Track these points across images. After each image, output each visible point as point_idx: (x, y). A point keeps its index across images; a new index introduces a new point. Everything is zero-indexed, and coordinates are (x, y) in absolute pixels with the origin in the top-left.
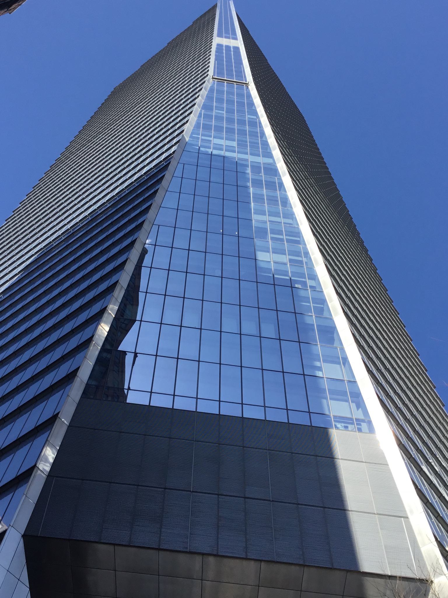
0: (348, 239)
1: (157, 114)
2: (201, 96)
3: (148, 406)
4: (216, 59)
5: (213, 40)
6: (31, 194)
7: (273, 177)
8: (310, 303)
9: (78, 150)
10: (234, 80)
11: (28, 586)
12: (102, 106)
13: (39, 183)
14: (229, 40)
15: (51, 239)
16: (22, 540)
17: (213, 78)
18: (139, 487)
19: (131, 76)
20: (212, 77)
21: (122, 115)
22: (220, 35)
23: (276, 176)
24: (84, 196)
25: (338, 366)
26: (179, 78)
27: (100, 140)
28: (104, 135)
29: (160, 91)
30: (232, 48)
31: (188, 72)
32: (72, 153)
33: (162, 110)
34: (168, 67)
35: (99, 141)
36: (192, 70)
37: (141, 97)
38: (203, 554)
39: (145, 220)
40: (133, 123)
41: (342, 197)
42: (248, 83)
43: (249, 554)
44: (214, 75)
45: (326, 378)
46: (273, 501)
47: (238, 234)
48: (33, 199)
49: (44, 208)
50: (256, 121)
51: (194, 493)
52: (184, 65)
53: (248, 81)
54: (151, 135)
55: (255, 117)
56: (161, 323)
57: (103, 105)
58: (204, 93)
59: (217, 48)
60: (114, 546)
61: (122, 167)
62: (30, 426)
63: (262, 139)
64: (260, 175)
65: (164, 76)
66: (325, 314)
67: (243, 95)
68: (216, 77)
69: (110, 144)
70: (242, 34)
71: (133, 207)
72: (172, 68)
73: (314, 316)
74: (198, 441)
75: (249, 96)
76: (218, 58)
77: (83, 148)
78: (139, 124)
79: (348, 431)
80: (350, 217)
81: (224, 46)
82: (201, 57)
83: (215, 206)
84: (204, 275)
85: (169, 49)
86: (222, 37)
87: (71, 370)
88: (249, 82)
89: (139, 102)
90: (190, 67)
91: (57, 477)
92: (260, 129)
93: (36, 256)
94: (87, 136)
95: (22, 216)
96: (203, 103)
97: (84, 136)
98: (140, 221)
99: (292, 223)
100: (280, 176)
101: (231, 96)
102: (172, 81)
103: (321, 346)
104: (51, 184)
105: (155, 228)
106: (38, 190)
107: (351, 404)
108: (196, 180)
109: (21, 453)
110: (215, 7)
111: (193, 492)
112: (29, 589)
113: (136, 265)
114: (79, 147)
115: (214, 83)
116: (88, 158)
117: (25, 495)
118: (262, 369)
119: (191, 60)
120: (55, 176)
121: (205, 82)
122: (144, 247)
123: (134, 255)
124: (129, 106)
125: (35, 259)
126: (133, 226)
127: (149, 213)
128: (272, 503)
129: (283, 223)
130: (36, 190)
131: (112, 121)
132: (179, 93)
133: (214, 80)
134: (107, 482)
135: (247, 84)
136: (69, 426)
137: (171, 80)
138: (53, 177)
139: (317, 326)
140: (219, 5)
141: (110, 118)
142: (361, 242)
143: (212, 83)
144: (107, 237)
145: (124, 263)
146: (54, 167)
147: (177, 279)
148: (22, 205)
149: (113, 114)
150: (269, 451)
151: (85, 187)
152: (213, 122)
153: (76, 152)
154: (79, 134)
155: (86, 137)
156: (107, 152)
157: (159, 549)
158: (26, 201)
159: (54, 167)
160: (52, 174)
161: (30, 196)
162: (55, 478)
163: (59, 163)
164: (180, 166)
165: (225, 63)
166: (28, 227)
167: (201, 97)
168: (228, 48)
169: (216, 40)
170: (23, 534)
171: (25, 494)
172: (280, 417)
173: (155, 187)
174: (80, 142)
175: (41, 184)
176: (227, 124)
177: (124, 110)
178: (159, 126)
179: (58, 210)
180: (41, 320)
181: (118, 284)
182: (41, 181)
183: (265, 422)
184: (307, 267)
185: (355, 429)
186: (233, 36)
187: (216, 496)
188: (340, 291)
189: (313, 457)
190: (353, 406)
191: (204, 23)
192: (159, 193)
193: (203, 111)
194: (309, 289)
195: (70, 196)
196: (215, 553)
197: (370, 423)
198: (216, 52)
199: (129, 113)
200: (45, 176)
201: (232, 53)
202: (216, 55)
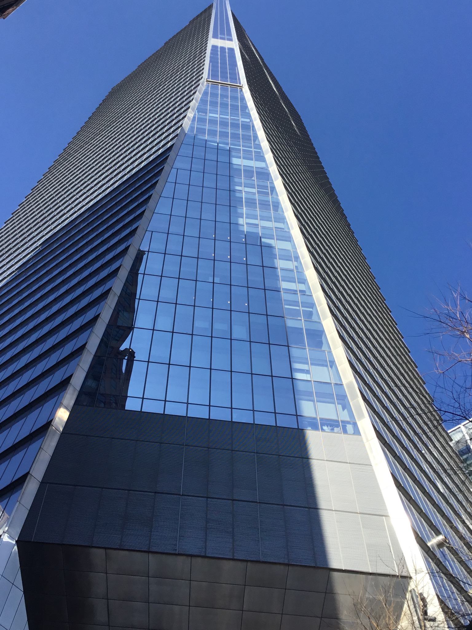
0: (342, 236)
3: (185, 416)
4: (210, 61)
5: (208, 42)
6: (29, 196)
7: (266, 181)
8: (299, 306)
10: (228, 82)
12: (99, 107)
13: (38, 185)
14: (225, 41)
17: (207, 81)
18: (130, 492)
19: (132, 73)
20: (206, 80)
21: (124, 112)
22: (215, 36)
23: (269, 181)
25: (325, 368)
26: (199, 60)
28: (81, 156)
29: (150, 97)
30: (227, 49)
32: (70, 155)
33: (164, 107)
34: (165, 67)
35: (108, 134)
36: (194, 67)
37: (137, 98)
39: (138, 227)
41: (337, 196)
42: (241, 85)
43: (235, 554)
44: (208, 78)
45: (313, 381)
46: (259, 503)
47: (230, 240)
48: (31, 201)
50: (248, 124)
51: (183, 497)
52: (174, 71)
54: (139, 144)
55: (248, 120)
56: (153, 330)
57: (100, 106)
58: (198, 96)
59: (212, 50)
60: (106, 551)
61: (126, 165)
63: (255, 142)
64: (252, 179)
65: (153, 85)
66: (314, 318)
67: (237, 98)
68: (210, 80)
69: (107, 146)
70: (237, 34)
71: (117, 220)
72: (167, 73)
73: (303, 320)
75: (243, 99)
76: (213, 60)
77: (80, 149)
79: (334, 433)
80: (344, 217)
81: (219, 48)
84: (196, 281)
85: (166, 50)
88: (243, 85)
89: (135, 103)
91: (50, 483)
92: (253, 132)
93: (8, 278)
94: (85, 138)
95: (21, 218)
96: (197, 107)
97: (85, 133)
98: (134, 227)
99: (283, 227)
100: (272, 180)
101: (225, 99)
103: (309, 350)
105: (148, 234)
106: (48, 184)
107: (337, 405)
108: (189, 185)
109: (17, 458)
110: (211, 7)
111: (182, 495)
112: (23, 593)
113: (129, 272)
114: (77, 148)
115: (208, 86)
117: (18, 502)
119: (198, 53)
120: (70, 165)
121: (199, 85)
122: (139, 248)
123: (127, 262)
124: (132, 103)
125: (6, 283)
126: (131, 217)
128: (258, 504)
130: (35, 192)
131: (131, 105)
133: (208, 83)
134: (99, 487)
137: (162, 87)
138: (52, 179)
139: (306, 330)
140: (214, 5)
141: (113, 116)
142: (354, 241)
143: (206, 86)
145: (118, 269)
146: (52, 168)
147: (169, 286)
148: (20, 208)
149: (110, 116)
150: (257, 454)
153: (74, 154)
154: (77, 135)
155: (84, 139)
156: (104, 155)
157: (149, 552)
158: (24, 203)
159: (52, 168)
160: (50, 176)
161: (29, 198)
162: (48, 484)
163: (57, 165)
165: (219, 65)
166: (26, 230)
167: (195, 101)
168: (223, 49)
169: (212, 42)
171: (19, 501)
172: (268, 420)
173: (149, 192)
174: (78, 144)
175: (39, 186)
176: (221, 128)
179: (56, 213)
180: (37, 325)
181: (111, 291)
182: (39, 183)
184: (297, 272)
185: (340, 431)
186: (228, 37)
187: (205, 499)
188: (330, 293)
190: (340, 407)
191: (174, 44)
194: (299, 293)
195: (67, 199)
196: (203, 555)
197: (355, 425)
198: (211, 53)
199: (126, 115)
200: (43, 178)
201: (227, 54)
202: (211, 57)
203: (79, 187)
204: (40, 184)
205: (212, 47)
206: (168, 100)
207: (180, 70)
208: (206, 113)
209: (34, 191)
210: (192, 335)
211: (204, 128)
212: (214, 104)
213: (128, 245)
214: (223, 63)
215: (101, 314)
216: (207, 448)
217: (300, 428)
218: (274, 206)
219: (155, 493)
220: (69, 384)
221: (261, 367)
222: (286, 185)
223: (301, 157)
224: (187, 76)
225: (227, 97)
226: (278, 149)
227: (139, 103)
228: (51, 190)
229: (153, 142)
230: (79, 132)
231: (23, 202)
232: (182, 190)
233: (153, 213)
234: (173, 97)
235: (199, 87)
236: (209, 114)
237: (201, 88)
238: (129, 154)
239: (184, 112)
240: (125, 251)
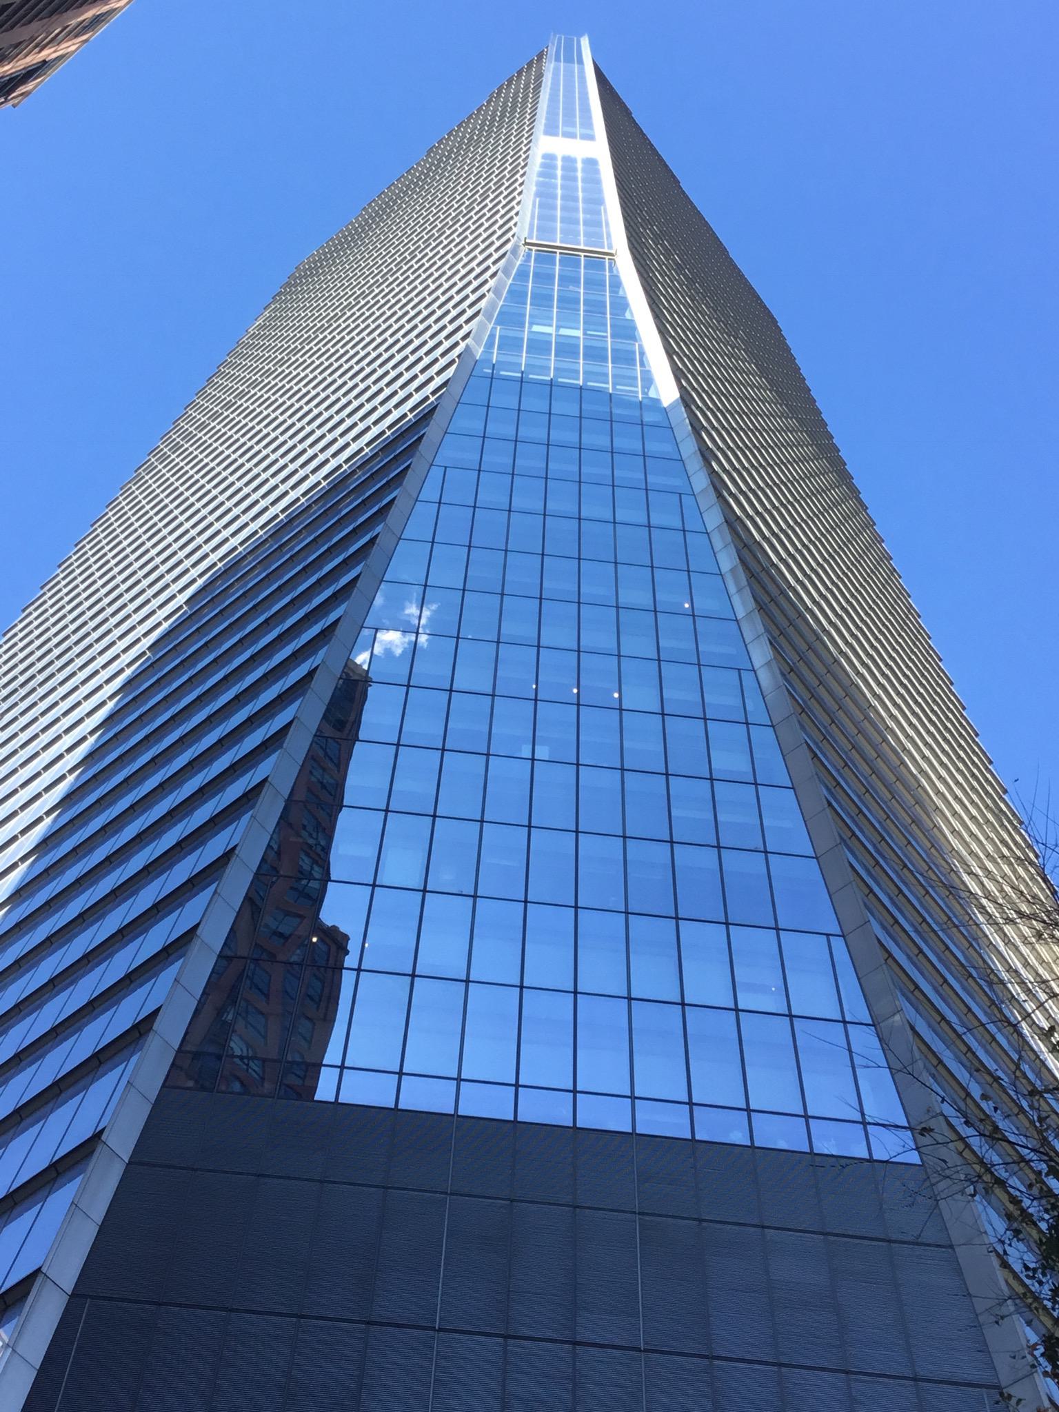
3: (391, 1109)
4: (538, 194)
22: (551, 130)
44: (531, 237)
46: (646, 1350)
53: (614, 248)
76: (545, 194)
83: (522, 574)
86: (556, 135)
87: (313, 667)
91: (92, 1297)
98: (333, 617)
101: (571, 288)
111: (440, 1330)
118: (630, 999)
126: (316, 630)
127: (351, 598)
134: (222, 1309)
135: (612, 255)
144: (307, 616)
150: (650, 1355)
152: (522, 356)
162: (88, 1300)
164: (436, 473)
167: (495, 295)
168: (569, 162)
169: (545, 145)
172: (671, 1124)
181: (267, 784)
183: (632, 1136)
187: (501, 1340)
189: (753, 1229)
192: (378, 545)
193: (499, 328)
208: (522, 325)
210: (475, 897)
211: (517, 361)
212: (542, 300)
214: (570, 197)
215: (238, 848)
217: (756, 1145)
219: (368, 1323)
220: (151, 1034)
223: (791, 413)
225: (576, 281)
226: (709, 408)
229: (72, 730)
230: (211, 378)
232: (455, 522)
233: (378, 582)
236: (530, 327)
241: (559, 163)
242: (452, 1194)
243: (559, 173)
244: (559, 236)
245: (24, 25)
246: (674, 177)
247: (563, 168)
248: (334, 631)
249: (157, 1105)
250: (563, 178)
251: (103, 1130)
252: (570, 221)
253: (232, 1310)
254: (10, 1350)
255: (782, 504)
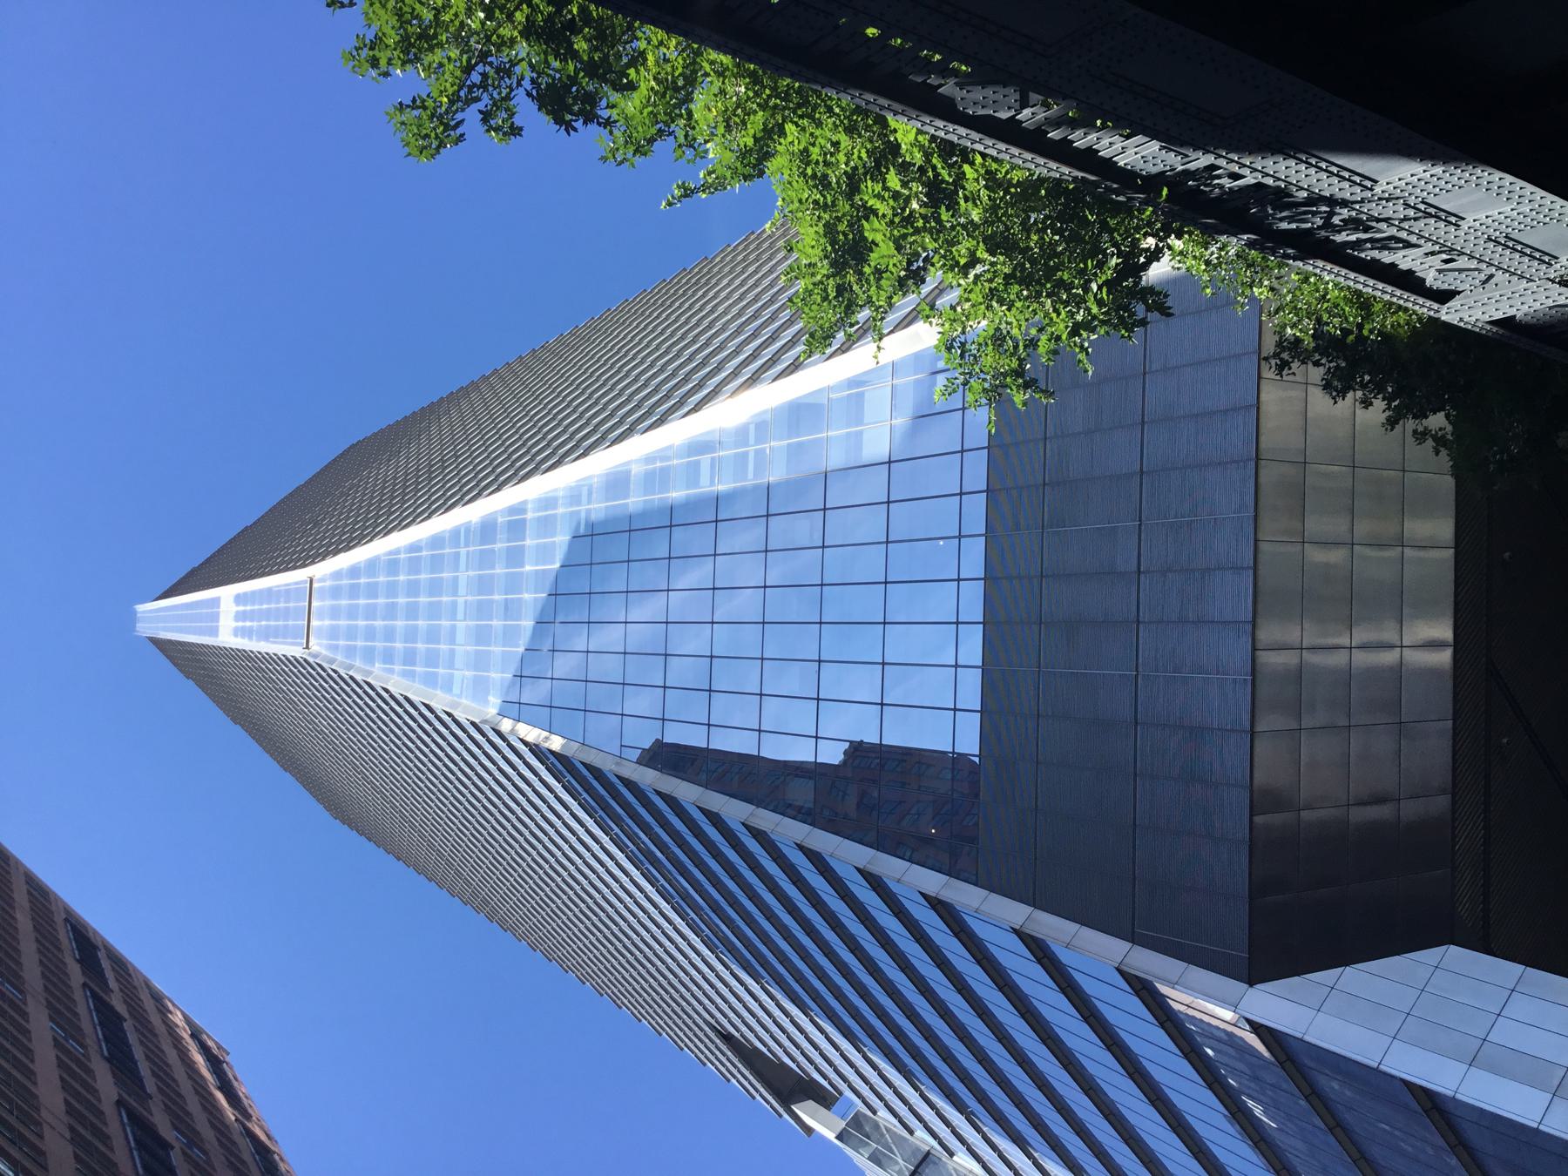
1: (362, 699)
2: (349, 670)
6: (564, 966)
9: (469, 884)
11: (1341, 969)
13: (541, 951)
15: (616, 887)
16: (1258, 986)
20: (307, 650)
22: (214, 632)
24: (527, 833)
27: (416, 814)
31: (274, 668)
32: (475, 894)
38: (1254, 649)
40: (387, 766)
49: (564, 903)
53: (306, 578)
62: (1037, 971)
72: (286, 710)
74: (1040, 664)
78: (387, 754)
82: (263, 667)
87: (926, 904)
89: (323, 737)
90: (285, 686)
91: (1133, 929)
94: (422, 849)
102: (282, 676)
104: (521, 910)
116: (452, 834)
126: (595, 784)
129: (589, 507)
132: (305, 669)
136: (1034, 906)
150: (1143, 518)
151: (509, 833)
158: (579, 974)
170: (1246, 986)
172: (977, 507)
177: (354, 774)
178: (387, 715)
181: (746, 822)
196: (1251, 626)
203: (512, 858)
204: (538, 947)
205: (217, 627)
206: (331, 704)
207: (278, 685)
209: (554, 958)
213: (744, 830)
214: (267, 615)
215: (796, 841)
216: (1040, 624)
218: (546, 509)
221: (871, 525)
222: (466, 497)
224: (301, 684)
227: (361, 770)
228: (525, 910)
231: (576, 975)
234: (323, 696)
235: (373, 682)
237: (342, 664)
238: (425, 765)
239: (416, 708)
240: (628, 783)
241: (240, 624)
242: (1039, 667)
243: (248, 624)
244: (300, 622)
245: (178, 1086)
246: (243, 531)
247: (244, 620)
248: (668, 796)
249: (992, 890)
250: (252, 620)
251: (795, 843)
252: (286, 614)
253: (1135, 824)
254: (1176, 986)
255: (499, 438)
